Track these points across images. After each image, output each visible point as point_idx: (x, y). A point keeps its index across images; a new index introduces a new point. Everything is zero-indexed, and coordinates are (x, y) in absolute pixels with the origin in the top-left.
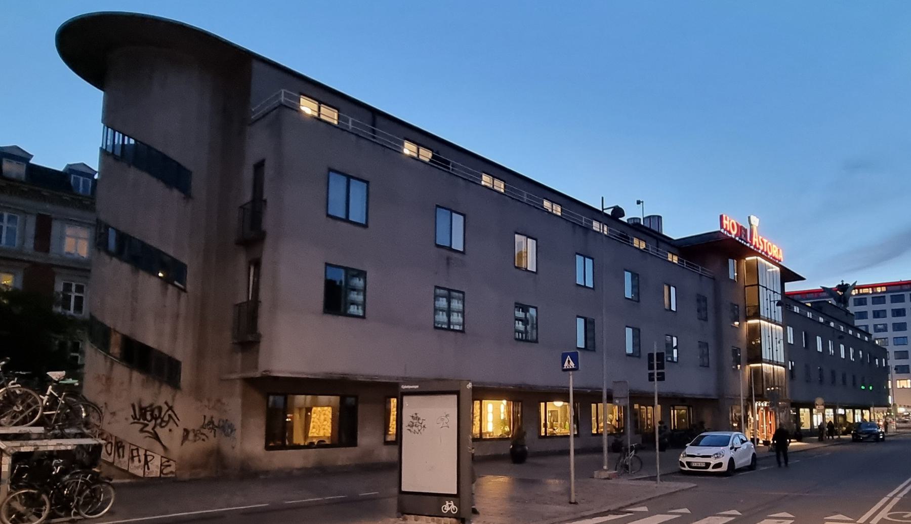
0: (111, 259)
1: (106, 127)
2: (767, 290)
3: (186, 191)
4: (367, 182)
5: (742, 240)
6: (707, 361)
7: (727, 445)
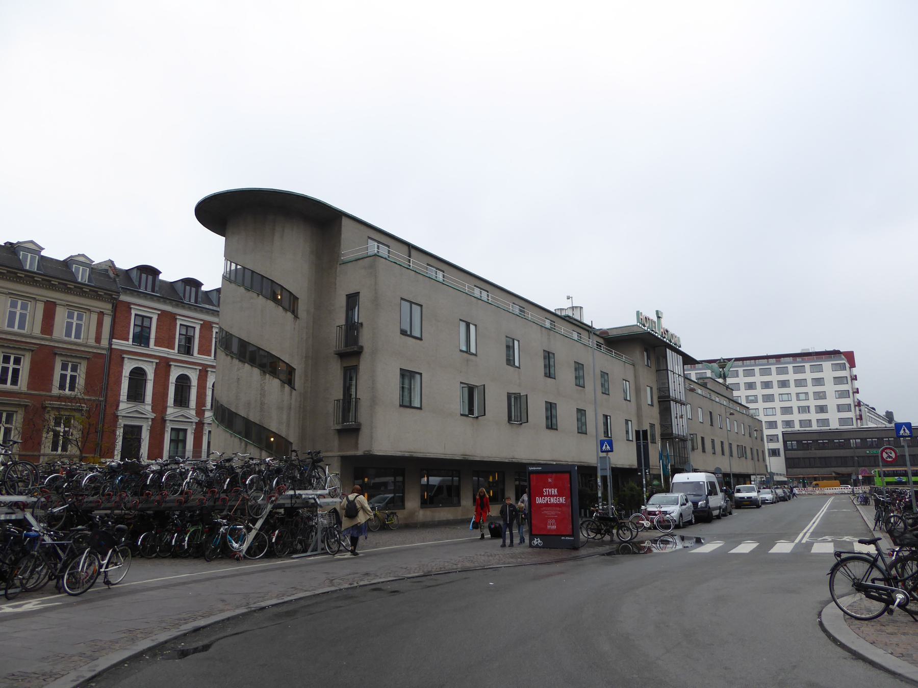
0: (244, 365)
1: (229, 262)
2: (673, 374)
3: (294, 312)
4: (421, 306)
5: (653, 331)
6: (585, 430)
7: (678, 504)
